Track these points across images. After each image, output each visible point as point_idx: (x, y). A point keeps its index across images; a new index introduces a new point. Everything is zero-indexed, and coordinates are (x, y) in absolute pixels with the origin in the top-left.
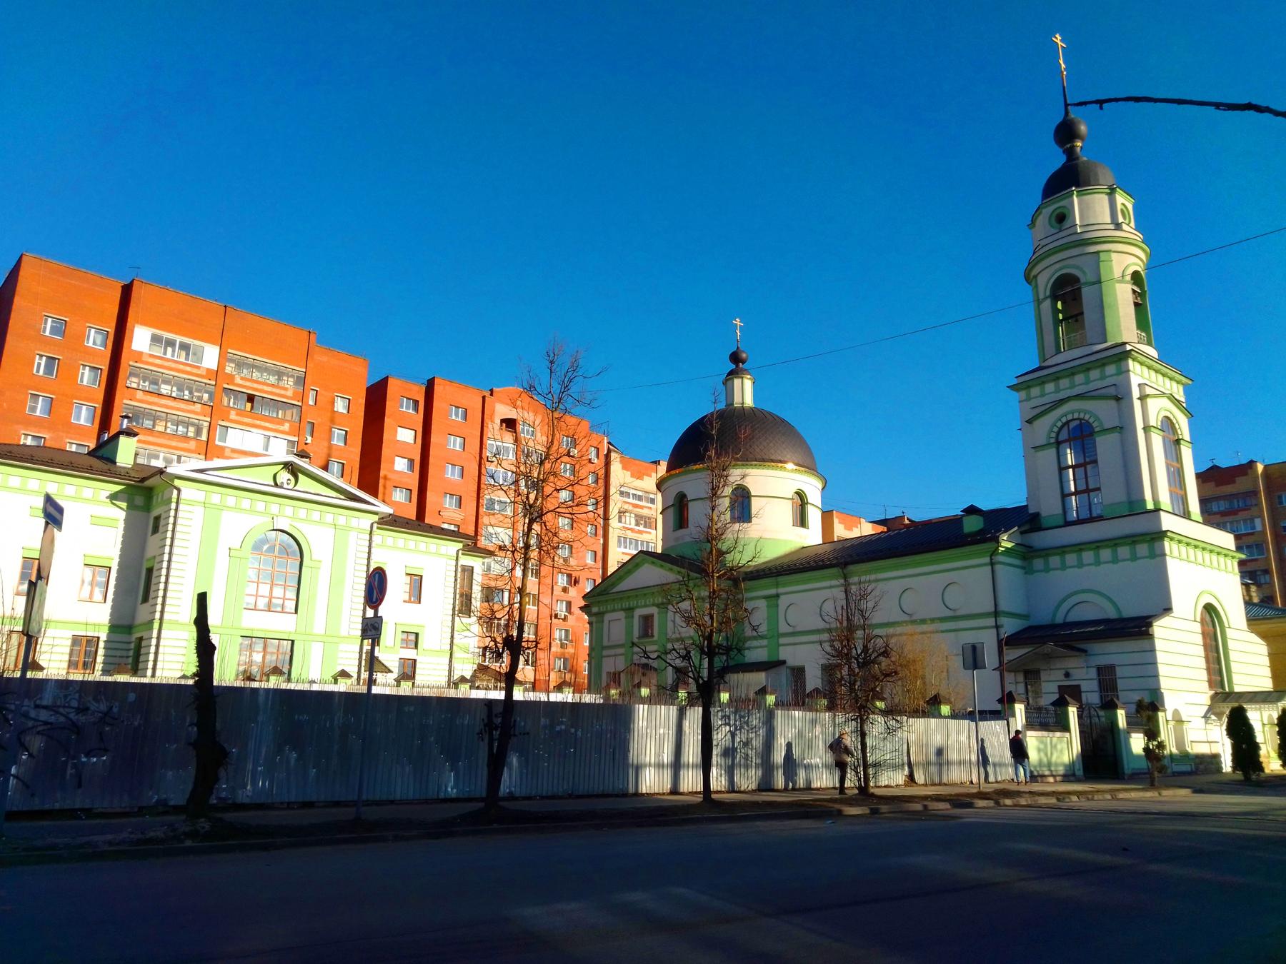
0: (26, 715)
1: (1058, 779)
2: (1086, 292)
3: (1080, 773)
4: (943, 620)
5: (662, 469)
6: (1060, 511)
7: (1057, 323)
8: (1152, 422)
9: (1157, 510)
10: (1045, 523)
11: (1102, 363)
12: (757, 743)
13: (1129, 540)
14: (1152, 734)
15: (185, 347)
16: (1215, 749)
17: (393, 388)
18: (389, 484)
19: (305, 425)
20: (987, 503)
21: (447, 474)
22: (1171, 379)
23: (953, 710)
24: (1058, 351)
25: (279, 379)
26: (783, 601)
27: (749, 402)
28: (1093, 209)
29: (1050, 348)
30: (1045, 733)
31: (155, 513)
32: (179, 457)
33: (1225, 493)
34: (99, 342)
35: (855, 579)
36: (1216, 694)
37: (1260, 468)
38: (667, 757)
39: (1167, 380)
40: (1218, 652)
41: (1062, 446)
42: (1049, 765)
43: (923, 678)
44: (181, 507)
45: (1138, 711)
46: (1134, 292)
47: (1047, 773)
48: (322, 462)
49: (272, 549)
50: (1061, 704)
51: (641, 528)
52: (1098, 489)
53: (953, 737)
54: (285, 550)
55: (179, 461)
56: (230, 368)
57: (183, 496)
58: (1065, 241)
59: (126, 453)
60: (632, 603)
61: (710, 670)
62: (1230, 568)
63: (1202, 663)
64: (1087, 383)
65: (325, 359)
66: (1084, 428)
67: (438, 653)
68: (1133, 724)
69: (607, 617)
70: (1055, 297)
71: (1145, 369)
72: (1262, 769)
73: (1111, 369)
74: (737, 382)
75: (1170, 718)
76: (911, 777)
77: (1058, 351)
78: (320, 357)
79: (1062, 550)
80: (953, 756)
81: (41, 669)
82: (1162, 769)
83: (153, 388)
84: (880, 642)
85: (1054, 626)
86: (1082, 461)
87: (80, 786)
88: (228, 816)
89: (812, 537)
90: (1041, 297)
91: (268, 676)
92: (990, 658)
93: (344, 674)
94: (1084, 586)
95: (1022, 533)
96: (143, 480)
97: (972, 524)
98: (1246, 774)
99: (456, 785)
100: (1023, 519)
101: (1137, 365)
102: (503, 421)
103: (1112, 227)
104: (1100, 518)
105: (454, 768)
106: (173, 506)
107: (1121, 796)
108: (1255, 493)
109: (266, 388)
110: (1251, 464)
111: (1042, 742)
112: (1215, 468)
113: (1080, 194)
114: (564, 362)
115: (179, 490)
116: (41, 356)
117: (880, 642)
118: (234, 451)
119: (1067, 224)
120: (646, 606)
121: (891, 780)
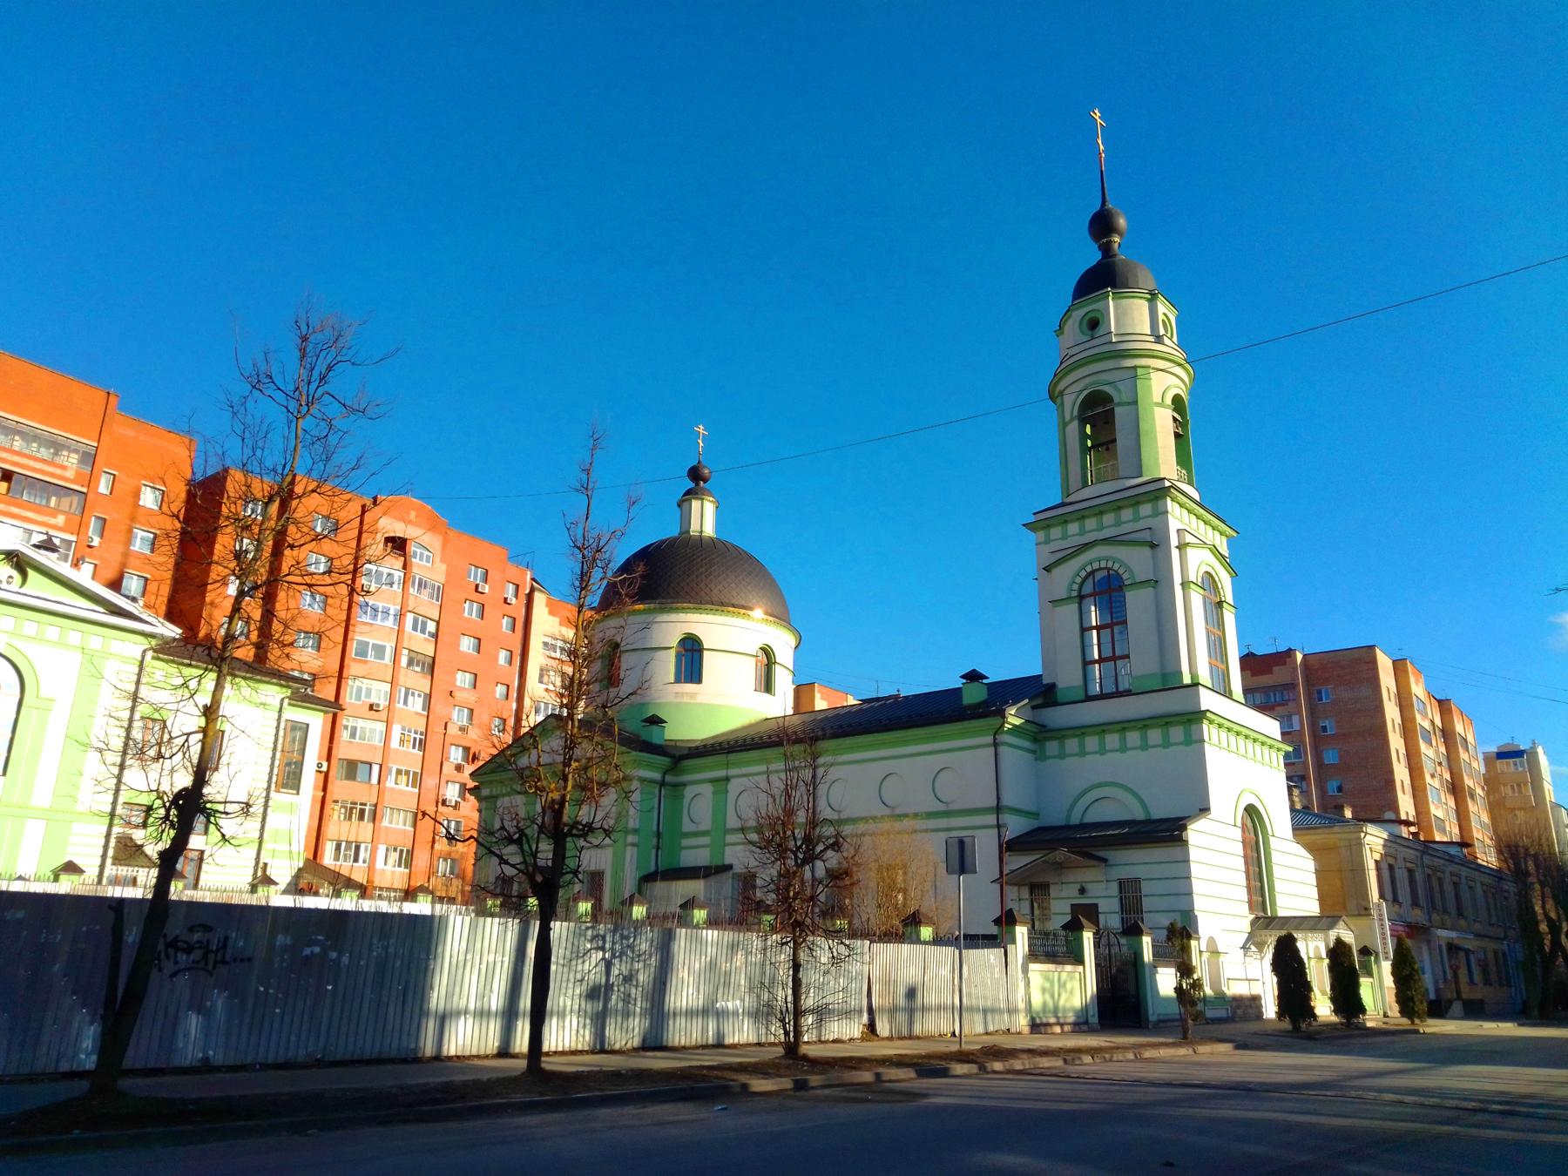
1: (1067, 1028)
2: (1119, 412)
3: (1094, 1020)
4: (931, 815)
6: (1080, 682)
7: (1085, 450)
10: (1061, 697)
14: (1185, 970)
16: (1255, 989)
20: (996, 673)
23: (936, 934)
24: (1085, 485)
26: (734, 787)
27: (709, 530)
28: (1132, 316)
29: (1075, 481)
30: (1051, 967)
33: (1266, 679)
36: (1257, 918)
37: (1299, 657)
38: (496, 1001)
41: (1085, 602)
42: (1056, 1010)
43: (905, 891)
45: (1169, 939)
46: (1175, 419)
47: (1052, 1020)
48: (111, 575)
50: (1074, 927)
52: (1127, 656)
66: (1112, 587)
68: (1161, 955)
70: (1083, 421)
72: (1315, 1016)
73: (1146, 509)
74: (695, 504)
75: (1203, 948)
76: (871, 1027)
78: (123, 429)
80: (931, 998)
82: (1198, 1017)
84: (828, 831)
85: (1068, 827)
89: (779, 705)
90: (1068, 418)
92: (985, 849)
93: (71, 868)
94: (1102, 779)
95: (1034, 708)
98: (1294, 1023)
100: (1038, 692)
102: (388, 540)
104: (1128, 693)
107: (1148, 1054)
108: (1293, 686)
109: (32, 463)
110: (1290, 653)
111: (1047, 979)
117: (828, 831)
119: (1100, 331)
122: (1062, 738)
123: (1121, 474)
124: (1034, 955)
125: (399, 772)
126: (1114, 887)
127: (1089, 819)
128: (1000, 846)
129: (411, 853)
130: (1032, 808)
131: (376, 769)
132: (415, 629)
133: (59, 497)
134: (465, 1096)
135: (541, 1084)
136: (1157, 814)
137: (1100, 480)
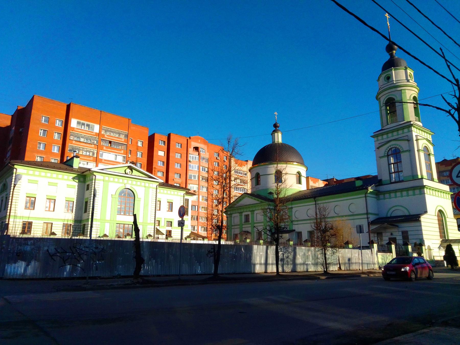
0: (82, 250)
5: (250, 164)
6: (389, 179)
7: (387, 114)
8: (420, 148)
9: (422, 178)
10: (384, 183)
11: (403, 128)
12: (291, 257)
13: (412, 189)
15: (88, 125)
17: (157, 137)
18: (156, 170)
19: (128, 151)
21: (175, 166)
22: (427, 133)
23: (353, 246)
24: (388, 124)
25: (119, 136)
26: (294, 210)
27: (280, 141)
29: (385, 123)
30: (384, 254)
31: (87, 183)
32: (87, 163)
34: (60, 124)
35: (319, 202)
36: (443, 240)
38: (263, 261)
39: (426, 134)
40: (443, 226)
43: (343, 235)
44: (96, 181)
49: (125, 195)
50: (389, 244)
51: (242, 184)
52: (402, 171)
53: (353, 255)
54: (129, 195)
55: (87, 164)
56: (103, 132)
57: (97, 178)
58: (389, 86)
59: (77, 164)
60: (242, 211)
61: (276, 234)
62: (448, 198)
63: (438, 230)
64: (398, 135)
65: (134, 128)
67: (192, 231)
68: (413, 251)
69: (233, 215)
70: (386, 106)
71: (418, 130)
73: (406, 130)
74: (276, 134)
75: (426, 248)
76: (340, 268)
77: (388, 124)
78: (133, 128)
79: (390, 192)
80: (354, 261)
81: (55, 234)
83: (78, 139)
86: (396, 161)
87: (97, 270)
88: (145, 278)
89: (303, 187)
90: (382, 105)
91: (126, 236)
92: (365, 229)
93: (150, 235)
94: (397, 204)
95: (376, 186)
96: (83, 173)
97: (359, 183)
99: (201, 270)
101: (415, 129)
102: (194, 148)
103: (406, 81)
104: (402, 181)
105: (200, 265)
106: (94, 181)
112: (445, 160)
113: (395, 70)
114: (233, 142)
115: (95, 176)
116: (41, 130)
117: (330, 225)
118: (105, 160)
119: (390, 80)
120: (246, 211)
121: (333, 269)
122: (384, 194)
123: (398, 121)
124: (379, 251)
125: (202, 207)
126: (400, 233)
127: (393, 215)
128: (368, 223)
129: (207, 228)
130: (377, 212)
131: (197, 207)
132: (203, 170)
133: (121, 146)
134: (265, 278)
135: (278, 276)
136: (412, 213)
137: (392, 122)
